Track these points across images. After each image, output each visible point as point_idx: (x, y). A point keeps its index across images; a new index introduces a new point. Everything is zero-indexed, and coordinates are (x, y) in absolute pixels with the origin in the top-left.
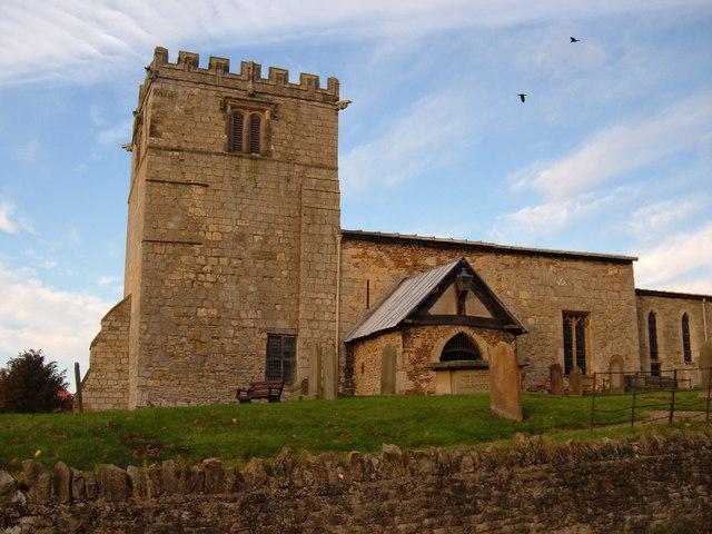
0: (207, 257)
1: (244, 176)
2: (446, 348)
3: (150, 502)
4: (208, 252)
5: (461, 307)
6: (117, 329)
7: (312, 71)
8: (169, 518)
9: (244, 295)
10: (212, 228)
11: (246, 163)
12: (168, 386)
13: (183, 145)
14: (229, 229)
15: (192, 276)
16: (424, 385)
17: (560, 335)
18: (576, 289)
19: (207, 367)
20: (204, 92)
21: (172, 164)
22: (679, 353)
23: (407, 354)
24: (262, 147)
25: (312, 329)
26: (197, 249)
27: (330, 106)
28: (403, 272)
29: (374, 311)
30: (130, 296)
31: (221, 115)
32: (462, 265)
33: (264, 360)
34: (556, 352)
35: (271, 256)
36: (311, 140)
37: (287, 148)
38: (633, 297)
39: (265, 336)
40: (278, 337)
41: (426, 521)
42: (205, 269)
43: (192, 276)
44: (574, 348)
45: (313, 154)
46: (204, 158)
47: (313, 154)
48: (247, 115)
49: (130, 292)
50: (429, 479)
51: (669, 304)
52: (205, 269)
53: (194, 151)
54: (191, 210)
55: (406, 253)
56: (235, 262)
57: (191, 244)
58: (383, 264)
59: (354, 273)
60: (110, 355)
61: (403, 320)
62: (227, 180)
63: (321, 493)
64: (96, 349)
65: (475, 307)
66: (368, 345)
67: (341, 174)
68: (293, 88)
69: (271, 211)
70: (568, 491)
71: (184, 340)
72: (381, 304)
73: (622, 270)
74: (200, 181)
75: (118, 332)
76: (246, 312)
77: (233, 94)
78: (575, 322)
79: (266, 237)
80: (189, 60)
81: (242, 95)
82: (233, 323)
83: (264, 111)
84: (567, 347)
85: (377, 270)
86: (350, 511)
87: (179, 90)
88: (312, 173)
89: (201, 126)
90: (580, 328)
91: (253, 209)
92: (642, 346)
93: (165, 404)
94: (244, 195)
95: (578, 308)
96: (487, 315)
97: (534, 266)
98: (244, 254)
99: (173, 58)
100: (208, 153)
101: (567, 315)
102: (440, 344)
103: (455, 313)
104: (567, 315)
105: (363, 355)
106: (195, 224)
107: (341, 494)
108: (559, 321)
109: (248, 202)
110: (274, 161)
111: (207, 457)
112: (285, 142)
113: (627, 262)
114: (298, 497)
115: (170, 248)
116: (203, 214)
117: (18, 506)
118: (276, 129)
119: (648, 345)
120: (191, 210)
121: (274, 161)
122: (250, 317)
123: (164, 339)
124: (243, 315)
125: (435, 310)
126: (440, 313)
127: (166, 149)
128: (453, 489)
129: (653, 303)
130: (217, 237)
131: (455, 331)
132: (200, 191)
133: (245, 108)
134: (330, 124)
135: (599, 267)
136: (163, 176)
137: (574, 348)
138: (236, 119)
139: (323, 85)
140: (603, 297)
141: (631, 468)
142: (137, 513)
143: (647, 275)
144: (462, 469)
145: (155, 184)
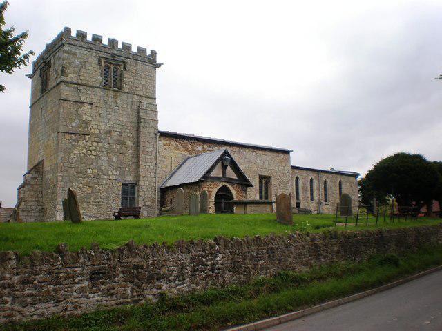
1: (110, 100)
5: (224, 173)
9: (110, 162)
10: (94, 127)
11: (111, 94)
13: (80, 82)
14: (103, 128)
24: (119, 85)
26: (87, 137)
28: (188, 154)
29: (175, 172)
32: (226, 153)
35: (123, 143)
38: (290, 170)
39: (121, 184)
40: (127, 185)
42: (91, 148)
44: (263, 193)
48: (112, 67)
52: (91, 148)
53: (85, 85)
54: (84, 117)
55: (189, 143)
58: (178, 149)
59: (164, 153)
65: (230, 173)
67: (158, 102)
68: (134, 54)
69: (124, 119)
72: (178, 169)
73: (286, 156)
77: (105, 55)
80: (82, 35)
81: (109, 56)
84: (261, 193)
85: (175, 153)
87: (77, 51)
88: (144, 100)
90: (267, 183)
91: (115, 117)
96: (235, 177)
101: (261, 177)
102: (215, 190)
104: (261, 177)
113: (287, 152)
115: (74, 137)
116: (90, 119)
118: (125, 76)
120: (84, 117)
122: (113, 174)
125: (212, 174)
130: (97, 131)
131: (221, 184)
132: (89, 107)
133: (110, 63)
135: (275, 154)
136: (70, 98)
137: (263, 193)
138: (107, 68)
139: (148, 53)
143: (295, 160)
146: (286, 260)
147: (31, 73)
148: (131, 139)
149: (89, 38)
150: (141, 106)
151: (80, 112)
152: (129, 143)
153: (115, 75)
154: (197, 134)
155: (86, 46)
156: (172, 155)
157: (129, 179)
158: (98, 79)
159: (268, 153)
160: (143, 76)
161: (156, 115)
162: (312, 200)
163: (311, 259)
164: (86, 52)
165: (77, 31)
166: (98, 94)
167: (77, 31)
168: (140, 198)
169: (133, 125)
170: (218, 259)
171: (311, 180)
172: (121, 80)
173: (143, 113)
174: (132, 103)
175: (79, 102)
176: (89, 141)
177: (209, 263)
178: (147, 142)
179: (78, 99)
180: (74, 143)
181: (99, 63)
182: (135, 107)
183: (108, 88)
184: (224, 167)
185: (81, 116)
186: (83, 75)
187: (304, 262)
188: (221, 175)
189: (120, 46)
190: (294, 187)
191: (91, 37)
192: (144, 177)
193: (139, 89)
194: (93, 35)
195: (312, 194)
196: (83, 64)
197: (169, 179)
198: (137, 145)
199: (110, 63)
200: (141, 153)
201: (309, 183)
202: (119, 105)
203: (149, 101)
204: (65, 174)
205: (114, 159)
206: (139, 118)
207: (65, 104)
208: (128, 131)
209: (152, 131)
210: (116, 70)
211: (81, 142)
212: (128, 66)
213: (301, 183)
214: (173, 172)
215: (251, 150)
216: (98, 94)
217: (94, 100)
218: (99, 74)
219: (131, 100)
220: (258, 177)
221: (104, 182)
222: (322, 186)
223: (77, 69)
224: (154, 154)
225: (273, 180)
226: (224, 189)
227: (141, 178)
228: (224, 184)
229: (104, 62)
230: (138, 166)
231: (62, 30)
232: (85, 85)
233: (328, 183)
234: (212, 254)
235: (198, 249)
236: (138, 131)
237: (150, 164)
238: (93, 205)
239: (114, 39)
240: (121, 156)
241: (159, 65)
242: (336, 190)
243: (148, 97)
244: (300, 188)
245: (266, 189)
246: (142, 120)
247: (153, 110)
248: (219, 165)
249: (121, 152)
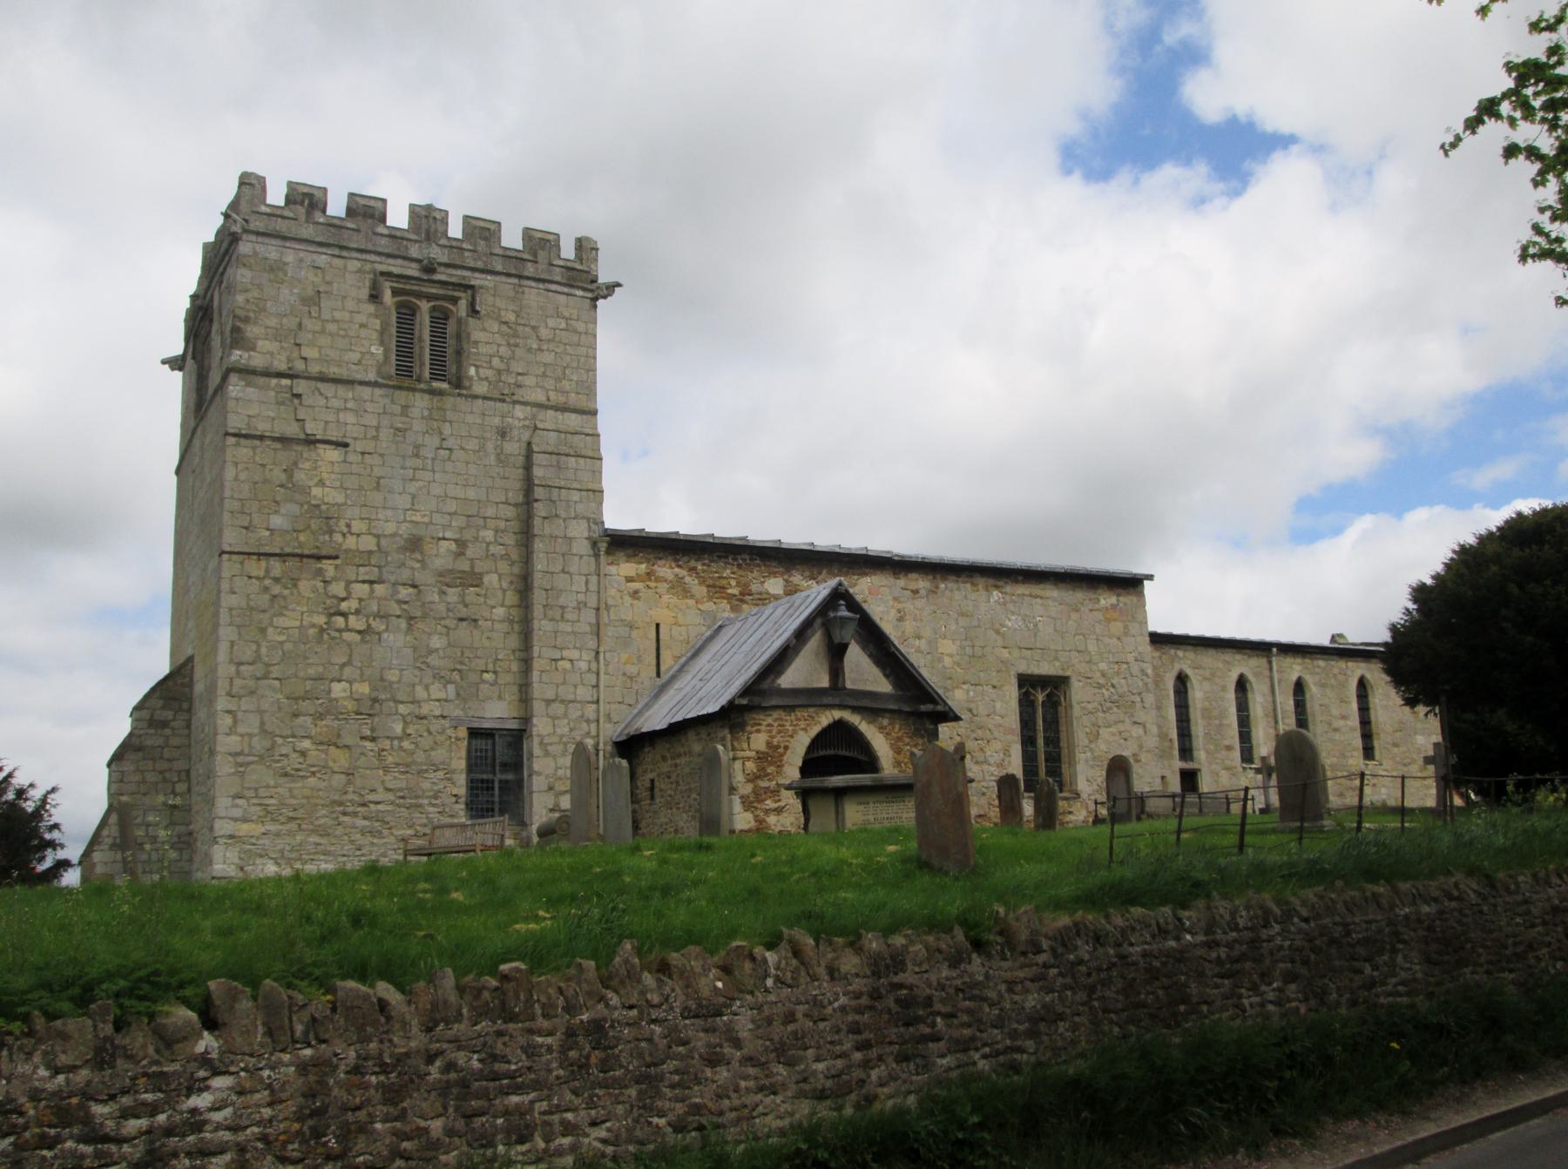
0: (348, 583)
1: (418, 426)
2: (816, 743)
3: (418, 1041)
4: (351, 572)
5: (836, 672)
6: (164, 724)
7: (540, 223)
8: (450, 1066)
9: (421, 655)
10: (357, 526)
11: (421, 403)
12: (278, 835)
13: (299, 366)
14: (390, 528)
15: (321, 620)
16: (772, 819)
17: (1013, 720)
18: (1042, 631)
19: (350, 796)
20: (337, 261)
21: (279, 403)
22: (1229, 748)
23: (738, 765)
24: (452, 369)
25: (554, 718)
26: (328, 567)
27: (580, 293)
28: (723, 610)
29: (673, 678)
30: (190, 659)
31: (371, 308)
32: (839, 596)
33: (462, 779)
34: (1007, 752)
35: (472, 579)
36: (548, 358)
37: (499, 372)
38: (1146, 647)
40: (488, 734)
41: (858, 1056)
42: (344, 606)
43: (321, 620)
44: (1041, 742)
45: (550, 384)
46: (342, 391)
47: (550, 384)
48: (425, 306)
49: (189, 652)
50: (857, 985)
51: (1210, 659)
52: (344, 606)
53: (323, 378)
54: (317, 491)
55: (728, 573)
56: (404, 592)
57: (319, 558)
58: (686, 593)
59: (627, 609)
60: (151, 777)
61: (731, 703)
62: (385, 434)
63: (687, 1013)
64: (128, 766)
65: (862, 671)
66: (662, 747)
67: (604, 423)
68: (509, 256)
69: (471, 494)
70: (1081, 996)
71: (306, 744)
72: (681, 670)
73: (1127, 600)
74: (333, 435)
75: (168, 731)
76: (427, 688)
77: (396, 267)
78: (1043, 699)
79: (462, 543)
80: (306, 199)
81: (413, 270)
82: (402, 709)
83: (455, 300)
84: (1028, 741)
85: (671, 605)
86: (737, 1043)
87: (290, 258)
88: (549, 419)
89: (332, 327)
90: (1053, 704)
91: (437, 490)
92: (1163, 736)
93: (271, 869)
94: (418, 463)
95: (1045, 669)
96: (883, 685)
97: (958, 593)
98: (420, 577)
99: (276, 196)
100: (350, 382)
101: (1028, 683)
102: (800, 744)
103: (825, 683)
104: (1028, 683)
105: (268, 727)
106: (327, 519)
107: (721, 1014)
108: (1012, 692)
109: (427, 476)
110: (476, 397)
111: (505, 961)
112: (496, 361)
113: (1131, 584)
114: (654, 1021)
115: (277, 567)
116: (340, 499)
117: (204, 1060)
118: (477, 335)
119: (1174, 735)
120: (317, 491)
121: (476, 397)
122: (435, 697)
123: (267, 744)
124: (420, 693)
125: (789, 679)
126: (800, 684)
127: (268, 373)
128: (898, 1001)
129: (1185, 660)
130: (368, 543)
131: (826, 719)
132: (333, 454)
133: (419, 295)
134: (580, 326)
135: (1079, 596)
136: (262, 427)
137: (1041, 742)
138: (406, 314)
139: (568, 251)
140: (1092, 647)
141: (1180, 956)
142: (400, 1059)
143: (1165, 610)
144: (910, 966)
145: (243, 441)
146: (690, 1077)
147: (177, 348)
148: (503, 567)
149: (336, 207)
150: (535, 440)
151: (300, 476)
152: (491, 580)
153: (438, 333)
154: (760, 533)
155: (384, 244)
156: (662, 615)
157: (497, 711)
158: (368, 348)
159: (1051, 592)
160: (544, 333)
161: (597, 473)
162: (1247, 756)
163: (866, 1065)
164: (322, 260)
165: (290, 184)
166: (369, 407)
167: (290, 184)
168: (538, 783)
169: (510, 512)
170: (201, 1101)
171: (1242, 685)
172: (459, 353)
173: (548, 466)
174: (503, 433)
175: (298, 441)
176: (335, 579)
177: (134, 1125)
178: (567, 575)
179: (292, 430)
180: (276, 589)
181: (375, 297)
182: (514, 448)
183: (407, 382)
184: (836, 653)
185: (306, 491)
186: (312, 344)
187: (821, 1082)
188: (825, 683)
189: (455, 230)
190: (1171, 713)
191: (284, 190)
192: (549, 702)
193: (529, 381)
194: (292, 186)
195: (1245, 737)
196: (313, 300)
197: (647, 706)
198: (525, 585)
199: (419, 295)
200: (538, 611)
201: (1231, 695)
202: (450, 443)
203: (573, 421)
204: (247, 703)
205: (437, 642)
206: (529, 485)
207: (244, 451)
208: (488, 535)
209: (579, 530)
210: (440, 318)
211: (305, 586)
212: (485, 302)
213: (1197, 694)
214: (665, 677)
215: (981, 581)
216: (369, 407)
217: (353, 431)
218: (375, 336)
219: (497, 421)
220: (1014, 682)
221: (398, 728)
222: (1287, 702)
223: (291, 323)
224: (590, 616)
225: (1078, 693)
226: (840, 733)
227: (538, 707)
228: (838, 714)
229: (395, 292)
230: (526, 663)
231: (227, 192)
232: (323, 378)
233: (1313, 690)
234: (159, 1081)
235: (63, 1059)
236: (526, 536)
237: (574, 654)
238: (355, 814)
239: (429, 207)
240: (463, 632)
241: (612, 288)
242: (1344, 717)
243: (563, 409)
244: (1196, 715)
245: (1053, 724)
246: (539, 492)
247: (585, 451)
248: (815, 642)
249: (464, 612)
